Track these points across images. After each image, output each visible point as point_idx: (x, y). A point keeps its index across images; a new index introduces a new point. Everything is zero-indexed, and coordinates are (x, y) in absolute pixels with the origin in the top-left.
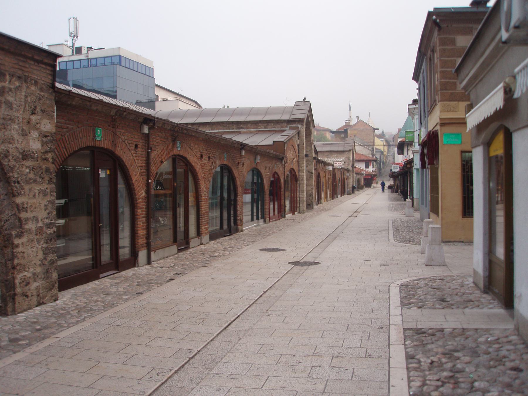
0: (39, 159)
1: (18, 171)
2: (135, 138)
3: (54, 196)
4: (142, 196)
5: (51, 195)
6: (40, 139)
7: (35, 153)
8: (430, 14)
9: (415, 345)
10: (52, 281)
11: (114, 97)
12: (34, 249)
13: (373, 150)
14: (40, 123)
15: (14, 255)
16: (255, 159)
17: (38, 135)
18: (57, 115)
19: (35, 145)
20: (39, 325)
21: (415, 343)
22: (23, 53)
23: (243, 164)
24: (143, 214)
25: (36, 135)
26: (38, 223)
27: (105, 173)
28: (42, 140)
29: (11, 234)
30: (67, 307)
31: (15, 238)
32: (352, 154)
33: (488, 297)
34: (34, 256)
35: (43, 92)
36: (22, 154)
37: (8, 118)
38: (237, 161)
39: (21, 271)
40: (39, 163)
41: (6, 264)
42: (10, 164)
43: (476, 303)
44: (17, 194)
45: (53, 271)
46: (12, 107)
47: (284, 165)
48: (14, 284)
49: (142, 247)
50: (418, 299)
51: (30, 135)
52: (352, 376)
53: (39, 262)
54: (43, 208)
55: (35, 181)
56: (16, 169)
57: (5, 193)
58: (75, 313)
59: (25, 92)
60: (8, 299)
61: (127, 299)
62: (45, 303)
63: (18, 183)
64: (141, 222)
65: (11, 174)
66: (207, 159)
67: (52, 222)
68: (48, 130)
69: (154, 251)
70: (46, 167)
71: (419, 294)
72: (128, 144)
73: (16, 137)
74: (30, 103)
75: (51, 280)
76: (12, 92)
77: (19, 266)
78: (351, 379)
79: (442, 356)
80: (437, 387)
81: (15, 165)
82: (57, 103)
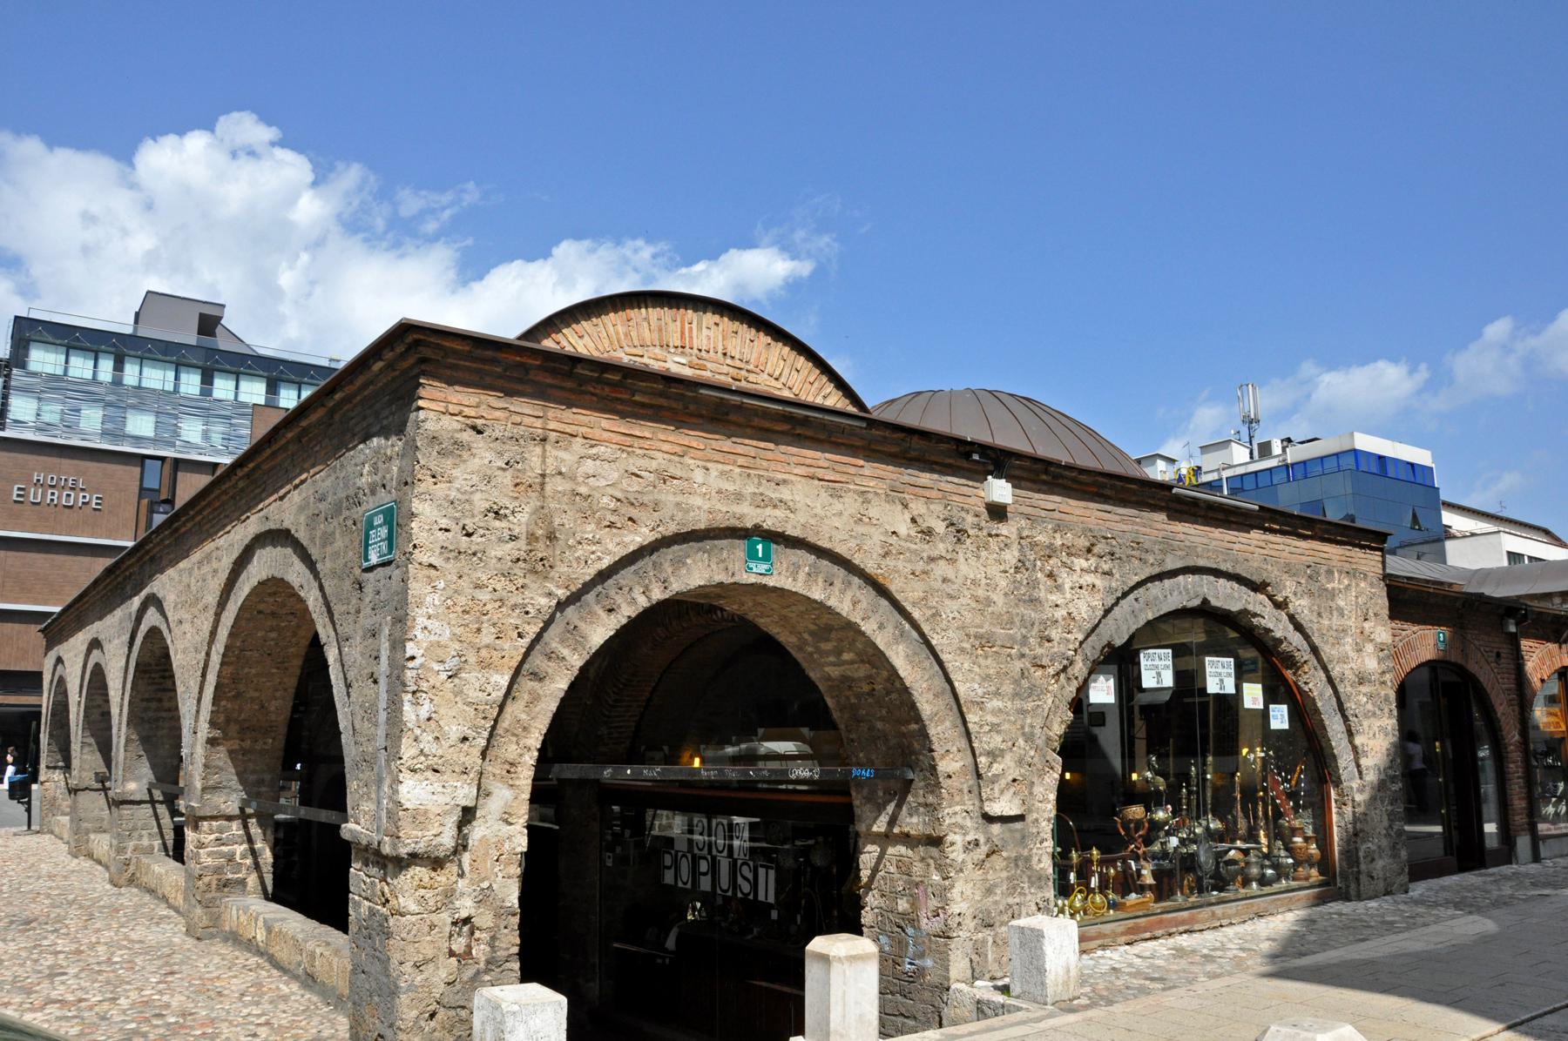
48: (1358, 858)
55: (1374, 714)
60: (1351, 877)
70: (1386, 695)
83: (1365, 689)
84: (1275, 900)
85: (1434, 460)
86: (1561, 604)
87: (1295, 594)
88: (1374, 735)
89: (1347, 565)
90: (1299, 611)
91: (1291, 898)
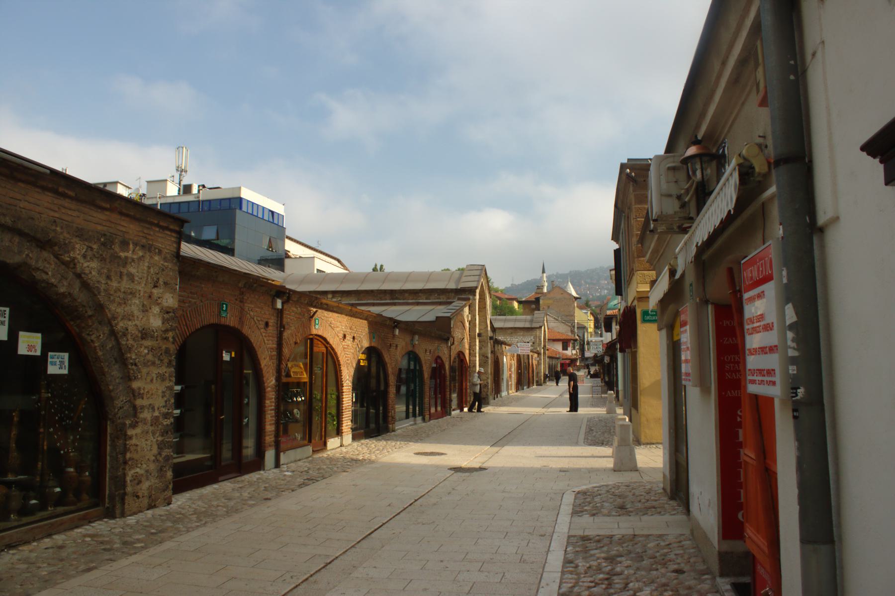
0: (159, 338)
1: (136, 351)
2: (265, 314)
3: (173, 381)
4: (271, 384)
5: (170, 380)
6: (161, 316)
7: (155, 331)
8: (623, 167)
9: (577, 551)
10: (166, 481)
11: (229, 251)
12: (149, 443)
13: (574, 327)
14: (161, 297)
15: (126, 448)
16: (412, 340)
17: (159, 311)
18: (179, 287)
19: (156, 322)
20: (154, 529)
21: (578, 549)
22: (148, 219)
23: (397, 346)
24: (272, 406)
25: (157, 312)
26: (154, 411)
27: (229, 356)
28: (163, 316)
29: (125, 424)
30: (183, 511)
31: (129, 428)
32: (543, 332)
33: (673, 503)
34: (148, 450)
35: (166, 262)
36: (141, 332)
37: (129, 291)
38: (388, 342)
39: (133, 467)
40: (159, 343)
41: (118, 458)
42: (128, 343)
43: (659, 510)
44: (133, 378)
45: (167, 468)
46: (134, 279)
47: (450, 347)
48: (125, 482)
49: (270, 446)
50: (593, 507)
51: (150, 311)
52: (502, 579)
53: (154, 458)
54: (161, 394)
55: (153, 363)
56: (134, 349)
57: (121, 376)
58: (194, 517)
59: (148, 262)
60: (117, 498)
61: (253, 504)
62: (158, 507)
63: (136, 365)
64: (269, 416)
65: (129, 355)
66: (352, 340)
67: (169, 411)
68: (170, 306)
69: (284, 451)
70: (166, 348)
71: (595, 502)
72: (257, 321)
73: (136, 313)
74: (152, 274)
75: (164, 479)
76: (135, 263)
77: (132, 461)
78: (500, 582)
79: (603, 561)
80: (589, 587)
81: (133, 344)
82: (181, 273)
83: (148, 343)
84: (32, 529)
85: (285, 212)
86: (332, 298)
87: (84, 256)
88: (152, 380)
89: (144, 241)
90: (87, 272)
91: (52, 524)
